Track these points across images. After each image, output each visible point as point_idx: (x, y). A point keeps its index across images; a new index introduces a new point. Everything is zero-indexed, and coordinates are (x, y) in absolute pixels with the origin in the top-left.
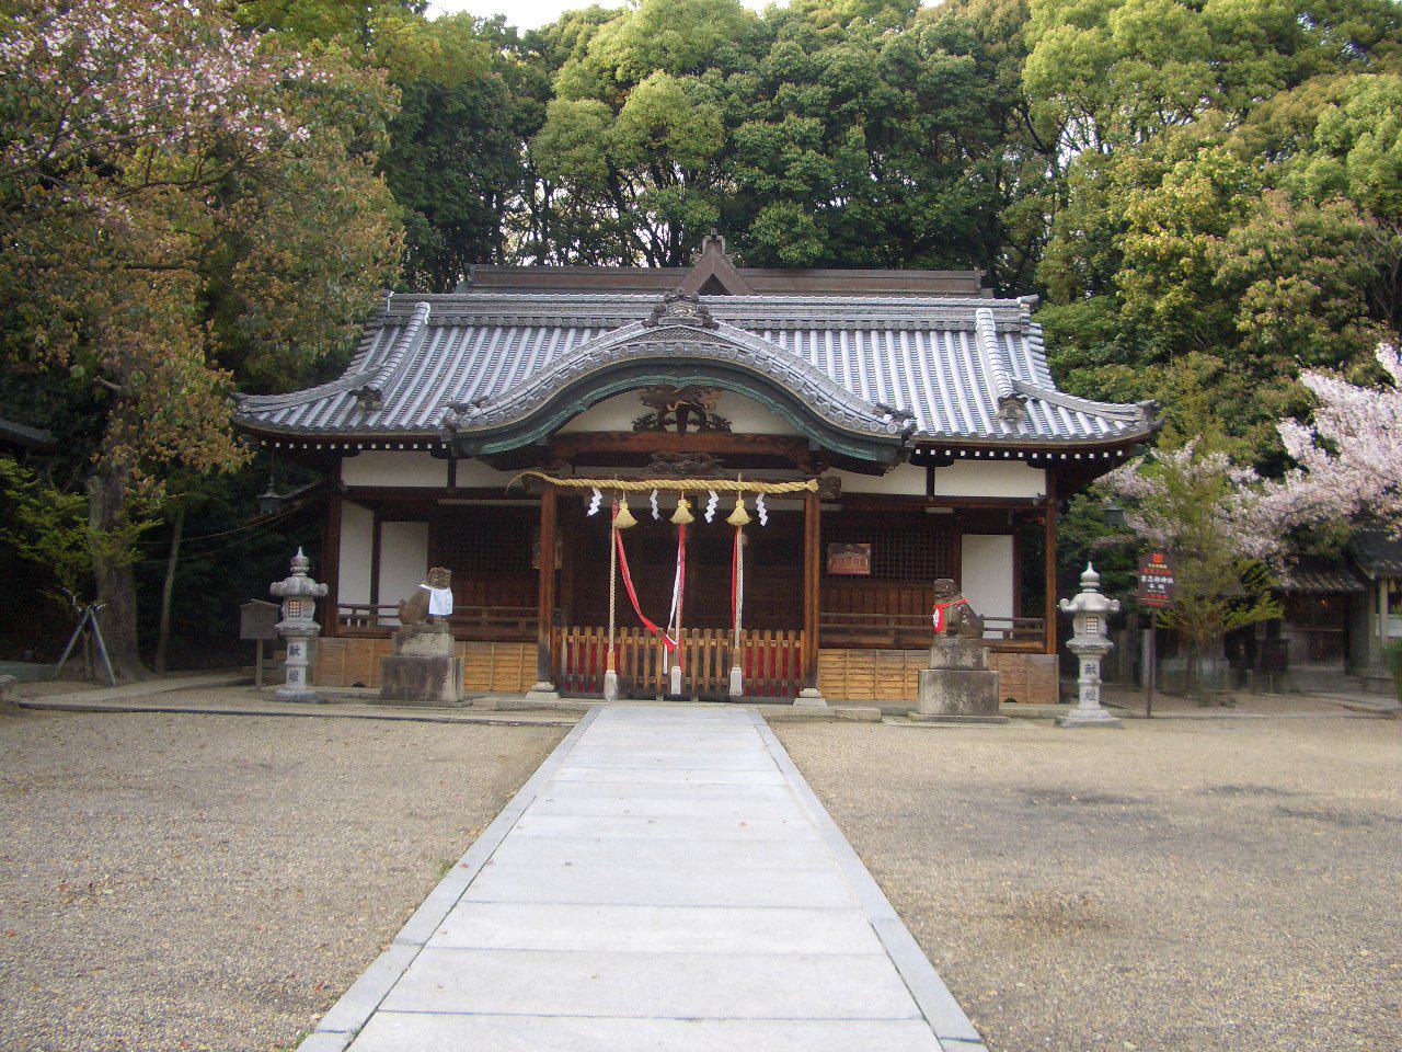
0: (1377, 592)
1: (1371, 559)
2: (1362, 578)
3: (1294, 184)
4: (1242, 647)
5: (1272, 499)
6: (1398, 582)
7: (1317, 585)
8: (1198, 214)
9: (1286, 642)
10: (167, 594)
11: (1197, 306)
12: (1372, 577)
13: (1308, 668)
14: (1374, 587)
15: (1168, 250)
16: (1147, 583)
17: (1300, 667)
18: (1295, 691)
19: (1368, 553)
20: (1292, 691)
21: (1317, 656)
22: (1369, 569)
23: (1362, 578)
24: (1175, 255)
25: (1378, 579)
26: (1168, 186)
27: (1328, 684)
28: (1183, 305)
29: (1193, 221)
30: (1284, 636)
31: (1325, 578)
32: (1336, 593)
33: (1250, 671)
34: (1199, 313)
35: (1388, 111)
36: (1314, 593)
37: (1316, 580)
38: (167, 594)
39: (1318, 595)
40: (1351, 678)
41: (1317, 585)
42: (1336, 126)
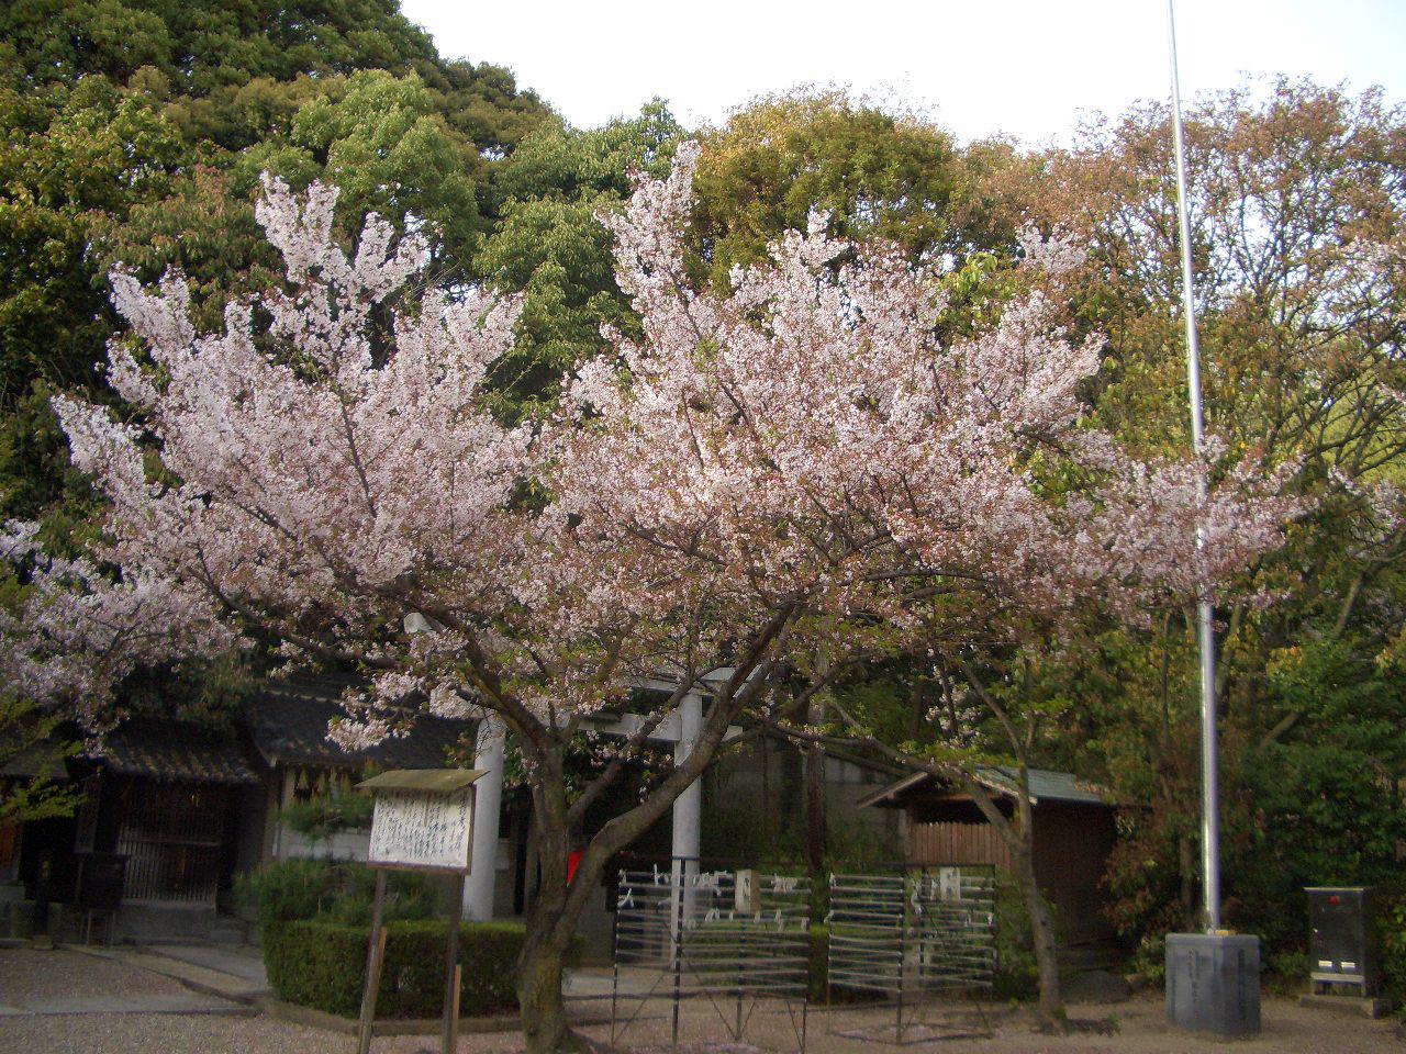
0: (281, 787)
1: (274, 736)
2: (258, 765)
3: (218, 466)
4: (46, 865)
5: (91, 600)
6: (3, 527)
7: (185, 770)
8: (91, 180)
9: (123, 860)
10: (1207, 711)
11: (66, 323)
12: (273, 763)
13: (158, 903)
14: (276, 778)
15: (31, 223)
16: (630, 584)
17: (141, 902)
18: (129, 942)
19: (271, 724)
20: (126, 941)
21: (174, 883)
22: (270, 751)
23: (258, 765)
24: (37, 236)
25: (281, 768)
26: (59, 135)
27: (188, 932)
28: (40, 315)
29: (82, 193)
30: (122, 849)
31: (200, 759)
32: (211, 787)
33: (57, 906)
34: (64, 331)
35: (396, 107)
36: (179, 780)
37: (187, 763)
38: (1207, 711)
39: (194, 785)
40: (225, 921)
41: (185, 770)
42: (322, 118)
